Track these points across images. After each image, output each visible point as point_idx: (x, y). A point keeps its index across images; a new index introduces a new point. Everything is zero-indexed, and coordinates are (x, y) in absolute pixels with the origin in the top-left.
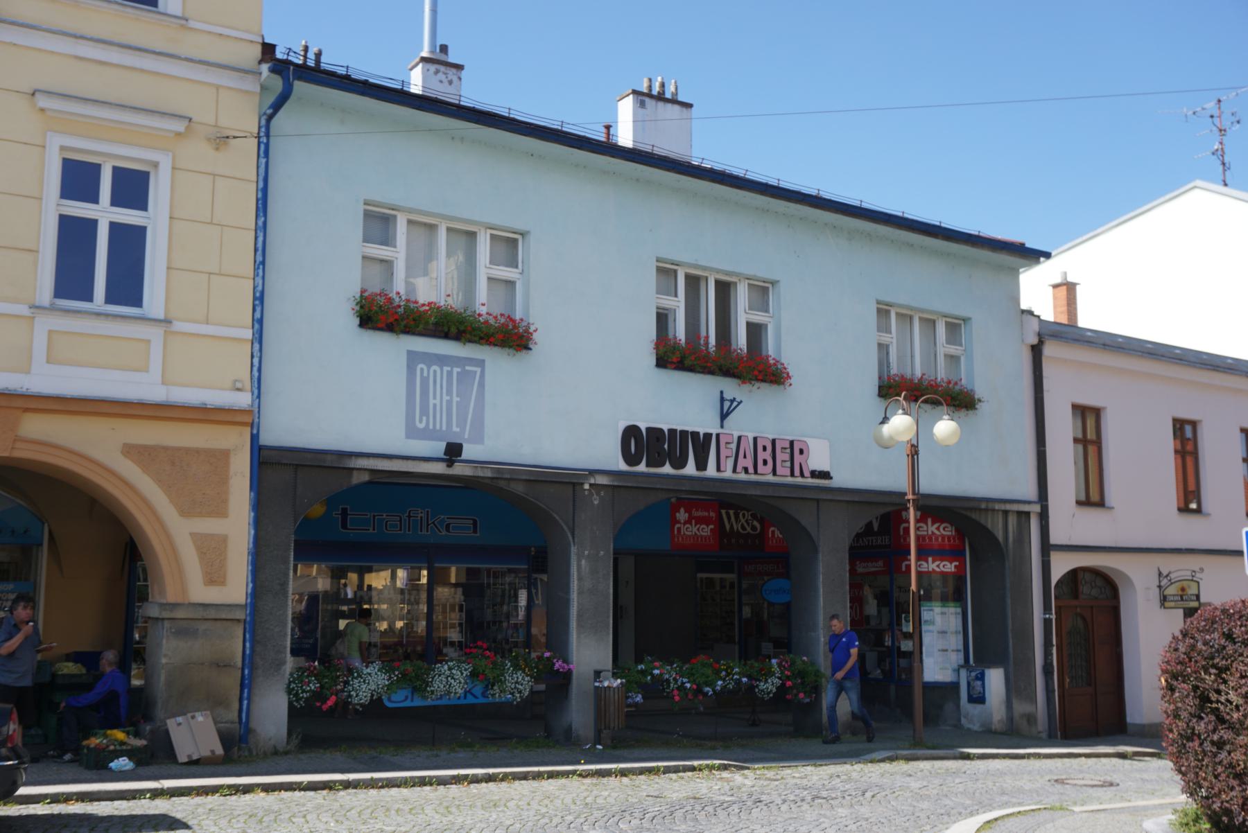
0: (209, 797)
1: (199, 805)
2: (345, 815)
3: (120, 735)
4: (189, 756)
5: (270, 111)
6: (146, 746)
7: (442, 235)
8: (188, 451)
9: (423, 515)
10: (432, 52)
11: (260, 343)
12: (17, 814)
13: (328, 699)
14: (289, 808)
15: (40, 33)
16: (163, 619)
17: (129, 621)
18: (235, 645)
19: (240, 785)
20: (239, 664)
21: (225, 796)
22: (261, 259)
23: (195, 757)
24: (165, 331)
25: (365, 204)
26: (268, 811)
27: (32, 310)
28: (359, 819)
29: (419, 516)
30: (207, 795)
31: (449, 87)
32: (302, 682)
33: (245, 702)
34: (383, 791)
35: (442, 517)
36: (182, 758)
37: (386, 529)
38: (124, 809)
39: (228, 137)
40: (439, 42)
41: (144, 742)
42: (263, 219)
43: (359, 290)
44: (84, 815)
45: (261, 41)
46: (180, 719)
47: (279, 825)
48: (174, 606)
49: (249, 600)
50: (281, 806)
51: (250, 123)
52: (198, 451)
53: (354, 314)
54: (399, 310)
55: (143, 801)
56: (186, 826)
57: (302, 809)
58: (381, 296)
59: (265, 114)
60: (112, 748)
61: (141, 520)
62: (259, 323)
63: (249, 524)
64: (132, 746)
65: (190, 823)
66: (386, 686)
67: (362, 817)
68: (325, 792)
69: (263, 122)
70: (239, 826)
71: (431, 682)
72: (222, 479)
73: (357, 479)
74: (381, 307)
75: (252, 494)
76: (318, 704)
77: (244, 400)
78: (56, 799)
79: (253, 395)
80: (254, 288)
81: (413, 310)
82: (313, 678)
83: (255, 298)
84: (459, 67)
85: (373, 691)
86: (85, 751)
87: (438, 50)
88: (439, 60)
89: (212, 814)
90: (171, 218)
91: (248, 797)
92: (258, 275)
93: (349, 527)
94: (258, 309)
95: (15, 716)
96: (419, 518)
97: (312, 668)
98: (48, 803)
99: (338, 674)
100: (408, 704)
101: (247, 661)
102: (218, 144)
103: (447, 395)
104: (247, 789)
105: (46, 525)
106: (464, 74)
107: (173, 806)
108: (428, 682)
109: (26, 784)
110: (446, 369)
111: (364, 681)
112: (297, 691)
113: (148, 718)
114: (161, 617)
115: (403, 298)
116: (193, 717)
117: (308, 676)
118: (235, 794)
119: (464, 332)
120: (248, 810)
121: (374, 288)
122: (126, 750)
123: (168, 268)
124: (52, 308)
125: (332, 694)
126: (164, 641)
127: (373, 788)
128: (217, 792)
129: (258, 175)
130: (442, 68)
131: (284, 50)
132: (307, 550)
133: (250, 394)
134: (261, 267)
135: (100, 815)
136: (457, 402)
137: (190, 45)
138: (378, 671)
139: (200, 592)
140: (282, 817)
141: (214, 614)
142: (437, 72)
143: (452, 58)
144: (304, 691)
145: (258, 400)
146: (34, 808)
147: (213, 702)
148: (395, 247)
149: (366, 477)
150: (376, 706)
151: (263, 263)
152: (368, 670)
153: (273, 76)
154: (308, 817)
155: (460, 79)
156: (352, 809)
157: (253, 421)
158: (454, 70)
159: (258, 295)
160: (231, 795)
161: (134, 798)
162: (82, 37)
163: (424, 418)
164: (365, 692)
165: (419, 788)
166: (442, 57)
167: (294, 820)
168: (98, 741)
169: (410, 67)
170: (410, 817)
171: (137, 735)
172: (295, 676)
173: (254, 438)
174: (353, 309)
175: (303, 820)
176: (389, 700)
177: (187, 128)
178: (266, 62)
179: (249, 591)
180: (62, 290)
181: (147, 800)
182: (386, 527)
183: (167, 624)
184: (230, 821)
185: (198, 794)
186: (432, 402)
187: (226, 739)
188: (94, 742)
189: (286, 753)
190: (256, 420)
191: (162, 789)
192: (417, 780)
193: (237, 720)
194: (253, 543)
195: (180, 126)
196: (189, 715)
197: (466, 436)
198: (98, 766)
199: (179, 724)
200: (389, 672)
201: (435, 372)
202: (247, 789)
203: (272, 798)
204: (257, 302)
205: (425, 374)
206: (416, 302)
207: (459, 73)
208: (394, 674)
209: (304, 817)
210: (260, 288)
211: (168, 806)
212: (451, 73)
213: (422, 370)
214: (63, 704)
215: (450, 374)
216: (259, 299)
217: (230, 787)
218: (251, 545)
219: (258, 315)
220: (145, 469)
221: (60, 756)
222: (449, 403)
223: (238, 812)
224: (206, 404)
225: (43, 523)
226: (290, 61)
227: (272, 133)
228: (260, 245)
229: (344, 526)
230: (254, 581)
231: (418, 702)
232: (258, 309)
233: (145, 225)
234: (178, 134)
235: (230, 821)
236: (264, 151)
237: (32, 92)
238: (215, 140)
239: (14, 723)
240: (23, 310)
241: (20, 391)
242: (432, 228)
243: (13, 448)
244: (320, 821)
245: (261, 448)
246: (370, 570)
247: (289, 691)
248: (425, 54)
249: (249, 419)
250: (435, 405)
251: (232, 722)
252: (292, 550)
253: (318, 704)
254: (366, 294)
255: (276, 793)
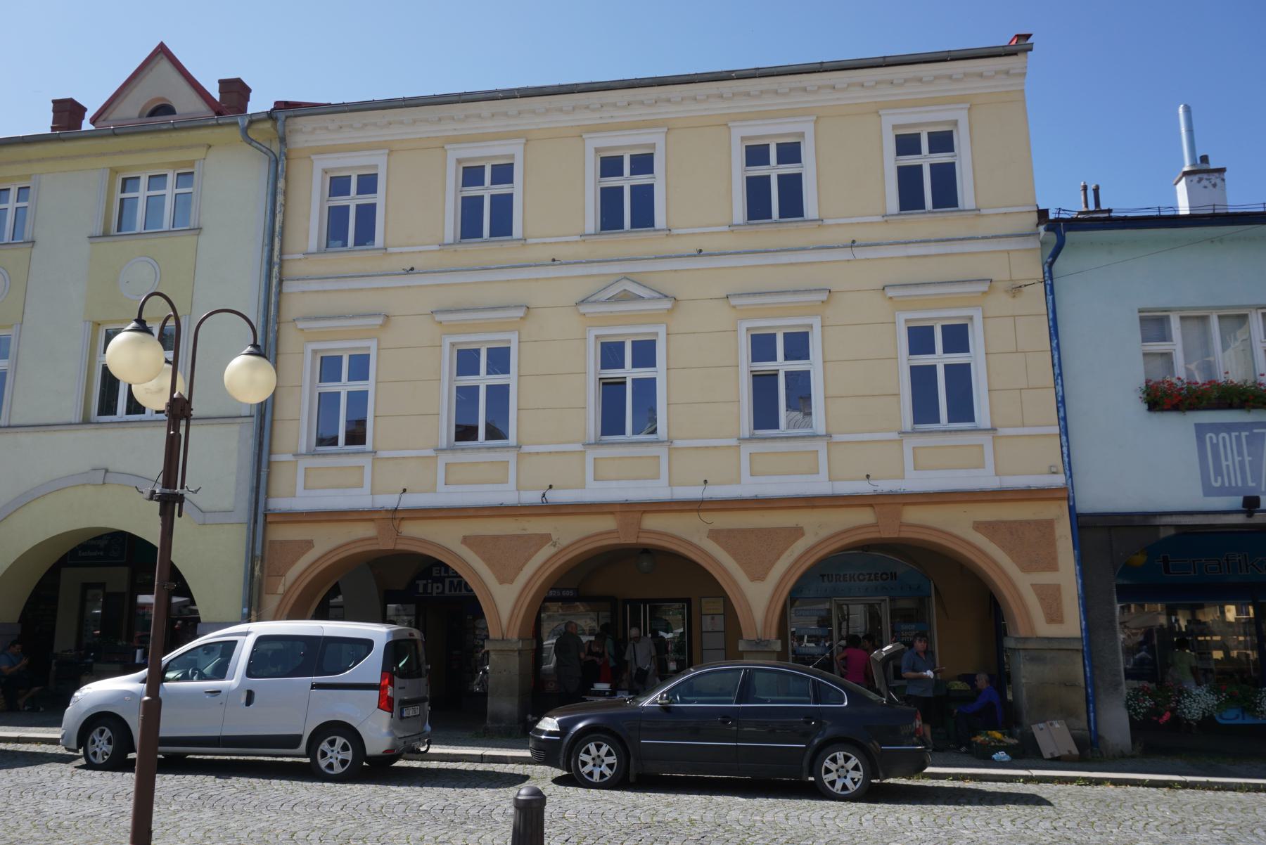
0: (1069, 785)
1: (1061, 790)
2: (1181, 808)
3: (998, 735)
4: (1052, 754)
5: (1050, 260)
6: (1017, 744)
7: (1214, 324)
8: (1021, 523)
9: (1240, 558)
10: (1193, 165)
11: (1067, 435)
12: (931, 785)
13: (1163, 715)
14: (1133, 798)
15: (882, 247)
16: (1019, 649)
17: (1000, 650)
18: (1077, 669)
19: (1093, 778)
20: (1083, 684)
21: (1081, 785)
22: (1059, 372)
23: (1056, 755)
24: (993, 437)
25: (1139, 312)
26: (1116, 799)
27: (901, 435)
28: (1193, 812)
29: (1237, 559)
30: (1067, 783)
31: (1214, 189)
32: (1137, 700)
33: (1092, 715)
34: (1219, 793)
35: (1260, 559)
36: (1047, 755)
37: (1206, 571)
38: (1004, 789)
39: (1020, 287)
40: (1199, 154)
41: (1016, 741)
42: (1056, 341)
43: (1144, 381)
44: (976, 789)
45: (1036, 209)
46: (1041, 725)
47: (1123, 810)
48: (1026, 639)
49: (1084, 635)
50: (1127, 797)
51: (1035, 271)
52: (1028, 523)
53: (1142, 401)
54: (1183, 392)
55: (1018, 784)
56: (1049, 804)
57: (1144, 800)
58: (1164, 384)
59: (1047, 262)
60: (993, 744)
61: (991, 573)
62: (1063, 421)
63: (1076, 575)
64: (1007, 743)
65: (1052, 802)
66: (1216, 705)
67: (1196, 810)
68: (1165, 790)
69: (1046, 269)
70: (1090, 807)
71: (1260, 703)
72: (1051, 542)
73: (1164, 534)
74: (1165, 392)
75: (1076, 552)
76: (1155, 718)
77: (1059, 480)
78: (956, 777)
79: (1066, 475)
80: (1056, 394)
81: (1195, 390)
82: (1147, 697)
83: (1057, 402)
84: (1222, 170)
85: (1203, 709)
86: (974, 745)
87: (1199, 161)
88: (1203, 171)
89: (1070, 797)
90: (986, 354)
91: (1100, 788)
92: (1058, 384)
93: (1171, 572)
94: (1062, 410)
95: (919, 716)
96: (1238, 561)
97: (1146, 689)
98: (951, 780)
99: (1170, 694)
100: (1239, 721)
101: (1089, 682)
102: (1014, 293)
103: (1239, 456)
104: (1099, 782)
105: (932, 582)
106: (1226, 175)
107: (1040, 789)
108: (1257, 703)
109: (933, 765)
110: (1234, 434)
111: (1194, 701)
112: (1135, 707)
113: (1018, 723)
114: (1017, 647)
115: (1185, 381)
116: (1051, 724)
117: (1143, 695)
118: (1089, 785)
119: (1247, 401)
120: (1099, 797)
121: (1157, 377)
122: (1003, 746)
123: (989, 391)
124: (914, 432)
125: (1166, 711)
126: (1022, 666)
127: (1209, 789)
128: (1075, 782)
129: (1047, 309)
130: (1205, 176)
131: (1055, 211)
132: (1126, 594)
133: (1063, 475)
134: (1059, 377)
135: (987, 790)
136: (1249, 461)
137: (984, 227)
138: (1207, 692)
139: (1045, 629)
140: (1126, 804)
141: (1057, 646)
142: (1200, 180)
143: (1213, 165)
144: (1140, 707)
145: (1070, 480)
146: (942, 783)
147: (1066, 713)
148: (1172, 341)
149: (1172, 532)
150: (1207, 723)
151: (1061, 374)
152: (1197, 692)
153: (1049, 233)
154: (1148, 807)
155: (1223, 180)
156: (1189, 803)
157: (1069, 495)
158: (1217, 175)
159: (1060, 399)
160: (1086, 785)
161: (1012, 781)
162: (910, 242)
163: (1219, 479)
164: (1195, 710)
165: (1254, 794)
166: (1204, 166)
167: (1135, 807)
168: (982, 738)
169: (1174, 183)
170: (1241, 814)
171: (1011, 735)
172: (1131, 694)
173: (1072, 509)
174: (1141, 398)
175: (1144, 808)
176: (1221, 717)
177: (990, 287)
178: (1042, 224)
179: (1083, 627)
180: (918, 419)
181: (1022, 784)
182: (1206, 571)
183: (1022, 653)
184: (1083, 803)
185: (1060, 783)
186: (1224, 463)
187: (1078, 742)
188: (980, 739)
189: (1133, 757)
190: (1071, 495)
191: (1032, 776)
192: (1251, 787)
193: (1087, 728)
194: (1082, 590)
195: (984, 287)
196: (1048, 722)
197: (1263, 489)
198: (984, 757)
199: (1042, 729)
200: (1216, 694)
201: (1224, 438)
202: (1099, 782)
203: (1119, 791)
204: (1060, 405)
205: (1215, 441)
206: (1196, 383)
207: (1221, 176)
208: (1221, 695)
209: (1145, 806)
210: (1060, 394)
211: (1038, 790)
212: (1213, 178)
213: (1211, 438)
214: (956, 711)
215: (1238, 438)
216: (1061, 402)
217: (1084, 779)
218: (1080, 591)
219: (1062, 414)
220: (992, 539)
221: (958, 748)
222: (1242, 463)
223: (1091, 798)
224: (1030, 487)
225: (930, 581)
226: (1062, 218)
227: (1054, 276)
228: (1056, 361)
229: (1167, 571)
230: (1086, 619)
231: (1249, 720)
232: (1062, 410)
233: (968, 362)
234: (984, 293)
235: (1083, 803)
236: (1050, 290)
237: (882, 288)
238: (1011, 291)
239: (919, 721)
240: (895, 436)
241: (899, 492)
242: (1204, 319)
243: (899, 531)
244: (1158, 809)
245: (1079, 516)
246: (1201, 607)
247: (1128, 707)
248: (1186, 169)
249: (1066, 494)
250: (1228, 466)
251: (1083, 730)
252: (1115, 594)
253: (1155, 718)
254: (1151, 383)
255: (1123, 787)
